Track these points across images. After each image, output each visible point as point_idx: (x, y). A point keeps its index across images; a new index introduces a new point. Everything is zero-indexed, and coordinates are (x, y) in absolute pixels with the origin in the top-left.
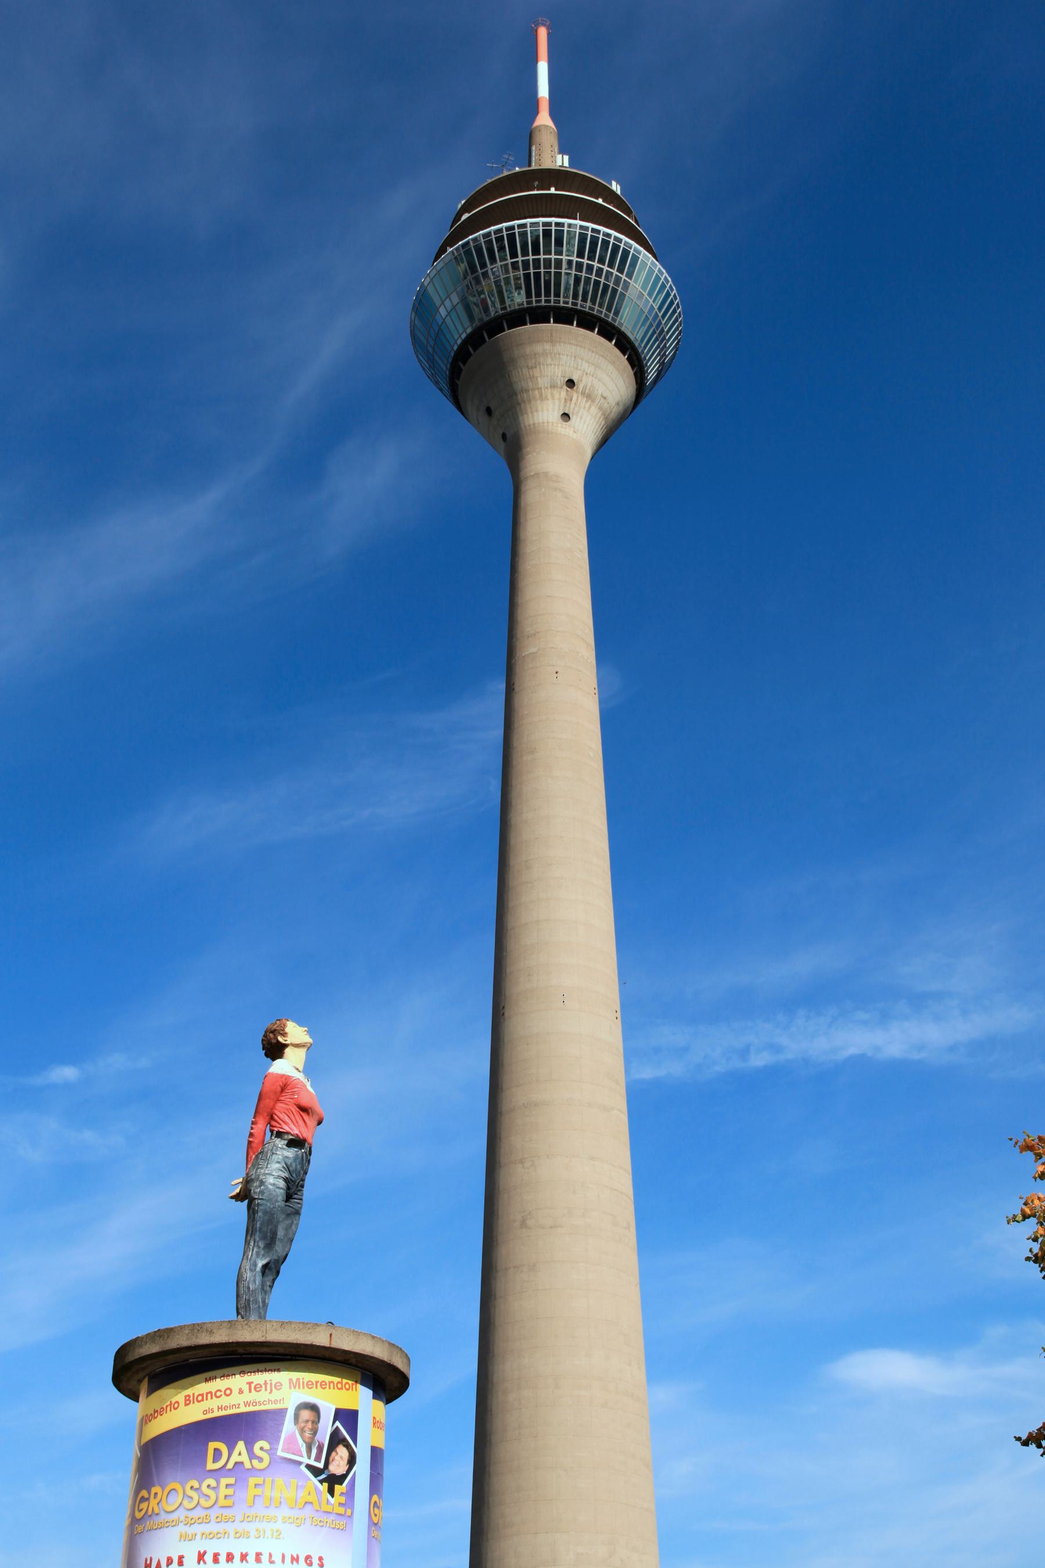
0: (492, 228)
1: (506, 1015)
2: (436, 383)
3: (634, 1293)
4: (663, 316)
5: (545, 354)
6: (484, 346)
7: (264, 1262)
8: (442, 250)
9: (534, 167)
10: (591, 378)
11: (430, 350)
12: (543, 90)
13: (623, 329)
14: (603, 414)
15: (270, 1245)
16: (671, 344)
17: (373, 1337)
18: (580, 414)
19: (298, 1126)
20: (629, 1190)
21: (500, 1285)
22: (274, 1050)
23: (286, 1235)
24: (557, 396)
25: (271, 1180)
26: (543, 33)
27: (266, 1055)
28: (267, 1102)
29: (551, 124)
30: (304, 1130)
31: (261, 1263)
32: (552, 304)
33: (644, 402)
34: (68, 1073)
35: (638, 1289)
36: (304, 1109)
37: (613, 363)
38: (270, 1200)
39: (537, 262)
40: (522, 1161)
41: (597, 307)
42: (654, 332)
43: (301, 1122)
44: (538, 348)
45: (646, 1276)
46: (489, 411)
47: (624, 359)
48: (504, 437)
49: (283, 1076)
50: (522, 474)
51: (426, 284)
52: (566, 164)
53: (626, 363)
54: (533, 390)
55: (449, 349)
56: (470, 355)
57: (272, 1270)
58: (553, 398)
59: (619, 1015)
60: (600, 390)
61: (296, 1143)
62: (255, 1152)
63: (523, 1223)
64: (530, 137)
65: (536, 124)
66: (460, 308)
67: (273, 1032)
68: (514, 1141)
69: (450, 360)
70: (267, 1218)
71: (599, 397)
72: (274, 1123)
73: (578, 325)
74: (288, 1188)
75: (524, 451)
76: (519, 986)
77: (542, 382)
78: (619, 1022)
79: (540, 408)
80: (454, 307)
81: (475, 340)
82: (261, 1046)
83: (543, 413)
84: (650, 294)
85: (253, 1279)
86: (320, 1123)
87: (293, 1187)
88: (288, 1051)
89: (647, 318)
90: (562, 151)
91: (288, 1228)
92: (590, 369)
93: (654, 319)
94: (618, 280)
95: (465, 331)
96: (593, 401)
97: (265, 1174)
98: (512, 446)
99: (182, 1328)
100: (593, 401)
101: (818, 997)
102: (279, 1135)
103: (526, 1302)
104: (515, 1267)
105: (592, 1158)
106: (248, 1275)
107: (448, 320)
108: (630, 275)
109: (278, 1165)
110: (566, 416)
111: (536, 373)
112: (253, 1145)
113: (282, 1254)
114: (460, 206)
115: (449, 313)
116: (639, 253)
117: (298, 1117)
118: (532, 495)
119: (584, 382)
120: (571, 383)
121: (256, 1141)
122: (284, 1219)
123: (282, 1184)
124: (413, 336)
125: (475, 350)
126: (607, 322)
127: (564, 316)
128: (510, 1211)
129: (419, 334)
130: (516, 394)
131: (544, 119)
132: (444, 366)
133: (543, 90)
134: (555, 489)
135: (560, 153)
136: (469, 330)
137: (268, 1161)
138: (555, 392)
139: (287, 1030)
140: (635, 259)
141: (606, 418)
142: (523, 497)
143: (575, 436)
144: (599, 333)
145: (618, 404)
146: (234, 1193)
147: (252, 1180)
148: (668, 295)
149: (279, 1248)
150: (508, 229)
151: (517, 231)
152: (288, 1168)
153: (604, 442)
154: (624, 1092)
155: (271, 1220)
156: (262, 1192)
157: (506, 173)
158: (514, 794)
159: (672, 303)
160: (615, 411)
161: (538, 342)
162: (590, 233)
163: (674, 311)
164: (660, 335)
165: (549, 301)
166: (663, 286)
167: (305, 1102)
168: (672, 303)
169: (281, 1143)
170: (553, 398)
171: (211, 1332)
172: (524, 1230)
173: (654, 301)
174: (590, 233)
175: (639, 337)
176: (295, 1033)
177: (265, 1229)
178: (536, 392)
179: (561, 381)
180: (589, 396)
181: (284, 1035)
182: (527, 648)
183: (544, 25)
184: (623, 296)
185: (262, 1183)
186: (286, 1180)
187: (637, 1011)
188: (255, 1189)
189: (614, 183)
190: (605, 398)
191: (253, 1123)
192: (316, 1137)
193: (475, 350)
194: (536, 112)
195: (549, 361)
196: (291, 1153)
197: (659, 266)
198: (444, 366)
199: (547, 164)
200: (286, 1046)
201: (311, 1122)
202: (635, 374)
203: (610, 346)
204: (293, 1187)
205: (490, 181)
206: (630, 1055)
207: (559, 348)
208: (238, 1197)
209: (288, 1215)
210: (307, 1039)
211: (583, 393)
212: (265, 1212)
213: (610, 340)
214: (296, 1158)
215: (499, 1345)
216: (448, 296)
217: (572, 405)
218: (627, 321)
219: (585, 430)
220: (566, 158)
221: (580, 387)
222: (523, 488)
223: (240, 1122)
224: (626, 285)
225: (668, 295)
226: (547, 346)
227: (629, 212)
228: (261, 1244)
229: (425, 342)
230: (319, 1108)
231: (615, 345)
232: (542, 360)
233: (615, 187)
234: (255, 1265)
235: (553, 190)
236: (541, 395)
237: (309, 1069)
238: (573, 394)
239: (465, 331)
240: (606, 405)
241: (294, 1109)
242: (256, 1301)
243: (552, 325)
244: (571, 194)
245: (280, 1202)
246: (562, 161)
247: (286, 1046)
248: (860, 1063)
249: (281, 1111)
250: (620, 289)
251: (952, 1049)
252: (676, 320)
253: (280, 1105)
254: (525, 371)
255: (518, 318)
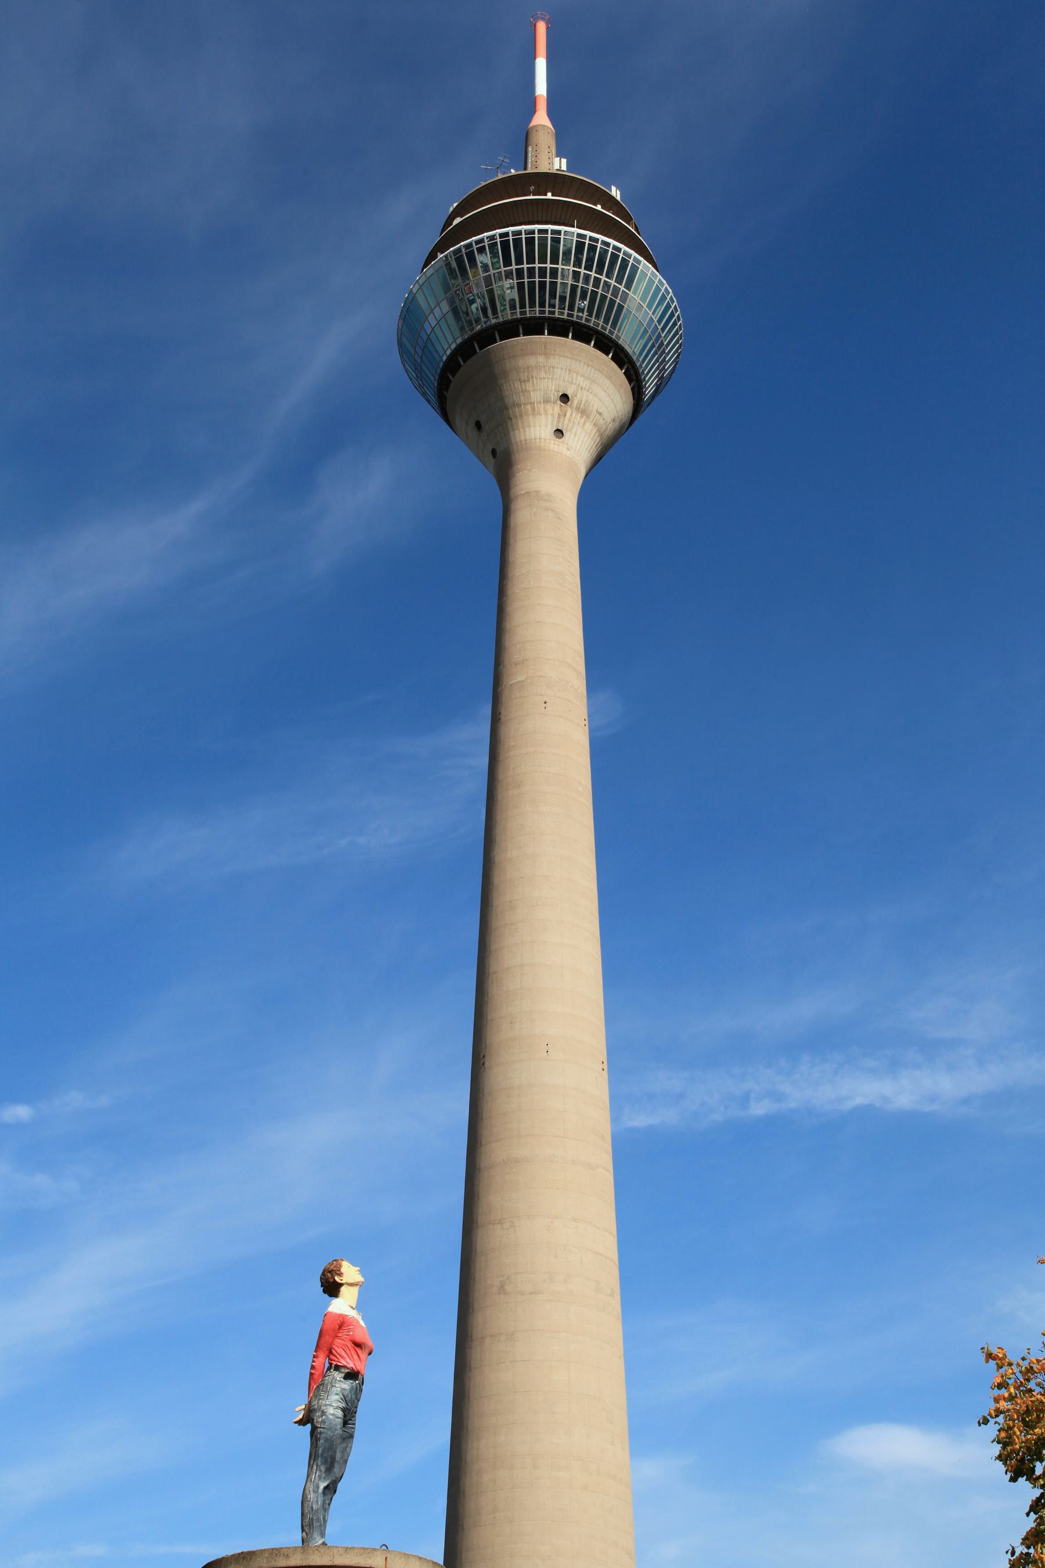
0: (486, 234)
1: (486, 1064)
2: (424, 394)
3: (617, 1365)
4: (663, 329)
5: (538, 367)
6: (474, 358)
7: (325, 1484)
8: (432, 256)
9: (529, 171)
10: (586, 393)
11: (419, 360)
12: (541, 88)
13: (620, 342)
14: (599, 430)
15: (329, 1469)
16: (671, 358)
17: (420, 1558)
18: (574, 431)
19: (351, 1357)
20: (613, 1253)
21: (475, 1355)
22: (332, 1288)
23: (342, 1457)
24: (550, 411)
25: (331, 1410)
26: (541, 27)
27: (324, 1292)
28: (327, 1338)
29: (548, 124)
30: (357, 1362)
31: (322, 1487)
32: (547, 315)
33: (640, 419)
34: (22, 1112)
35: (622, 1361)
36: (358, 1345)
37: (609, 378)
38: (330, 1429)
39: (531, 271)
40: (501, 1222)
41: (593, 319)
42: (653, 346)
43: (355, 1356)
44: (532, 361)
45: (630, 1339)
46: (478, 426)
47: (620, 373)
48: (494, 452)
49: (340, 1315)
50: (512, 492)
51: (414, 291)
52: (564, 168)
53: (624, 377)
54: (525, 404)
55: (438, 359)
56: (460, 366)
57: (331, 1489)
58: (546, 414)
59: (605, 1066)
60: (596, 405)
61: (352, 1375)
62: (316, 1384)
63: (502, 1289)
64: (526, 138)
65: (532, 124)
66: (450, 317)
67: (331, 1272)
68: (495, 1199)
69: (439, 371)
70: (327, 1445)
71: (594, 413)
72: (332, 1357)
73: (574, 338)
74: (345, 1416)
75: (515, 468)
76: (500, 1033)
77: (535, 396)
78: (605, 1074)
79: (532, 423)
80: (444, 316)
81: (465, 351)
82: (320, 1284)
83: (535, 429)
84: (649, 306)
85: (315, 1499)
86: (370, 1354)
87: (349, 1414)
88: (343, 1289)
89: (646, 331)
90: (559, 154)
91: (344, 1450)
92: (585, 384)
93: (653, 333)
94: (616, 290)
95: (455, 341)
96: (588, 417)
97: (326, 1405)
98: (502, 463)
99: (262, 1551)
100: (588, 417)
101: (824, 1042)
102: (337, 1368)
103: (501, 1375)
104: (492, 1336)
105: (575, 1220)
106: (311, 1496)
107: (437, 330)
108: (628, 286)
109: (337, 1397)
110: (559, 433)
111: (529, 386)
112: (315, 1376)
113: (338, 1475)
114: (451, 209)
115: (438, 322)
116: (639, 262)
117: (353, 1351)
118: (522, 514)
119: (579, 396)
120: (565, 398)
121: (317, 1373)
122: (341, 1443)
123: (340, 1413)
124: (400, 344)
125: (465, 362)
126: (604, 335)
127: (559, 329)
128: (488, 1274)
129: (406, 342)
130: (507, 408)
131: (541, 118)
132: (433, 378)
133: (541, 88)
134: (547, 509)
135: (557, 156)
136: (459, 341)
137: (328, 1392)
138: (549, 407)
139: (342, 1270)
140: (635, 269)
141: (601, 435)
142: (512, 517)
143: (568, 453)
144: (596, 346)
145: (614, 420)
146: (298, 1419)
147: (315, 1410)
148: (668, 306)
149: (336, 1469)
150: (502, 235)
151: (511, 238)
152: (345, 1399)
153: (599, 459)
154: (609, 1148)
155: (331, 1447)
156: (323, 1422)
157: (500, 176)
158: (498, 830)
159: (672, 315)
160: (611, 428)
161: (532, 354)
162: (587, 242)
163: (675, 324)
164: (660, 348)
165: (543, 312)
166: (664, 298)
167: (359, 1338)
168: (672, 315)
169: (338, 1376)
170: (546, 414)
171: (287, 1556)
172: (502, 1296)
173: (653, 314)
174: (587, 242)
175: (637, 350)
176: (350, 1273)
177: (326, 1455)
178: (529, 407)
179: (555, 395)
180: (584, 412)
181: (340, 1275)
182: (515, 676)
183: (543, 19)
184: (621, 307)
185: (323, 1413)
186: (344, 1410)
187: (624, 1056)
188: (318, 1418)
189: (614, 188)
190: (600, 414)
191: (314, 1356)
192: (368, 1367)
193: (465, 362)
194: (533, 111)
195: (543, 374)
196: (347, 1385)
197: (659, 277)
198: (433, 378)
199: (543, 168)
200: (341, 1285)
201: (363, 1355)
202: (633, 389)
203: (607, 360)
204: (349, 1414)
205: (484, 184)
206: (618, 1103)
207: (553, 361)
208: (301, 1422)
209: (344, 1439)
210: (359, 1278)
211: (578, 409)
212: (326, 1440)
213: (607, 354)
214: (352, 1389)
215: (474, 1422)
216: (438, 304)
217: (566, 421)
218: (627, 337)
219: (579, 447)
220: (564, 161)
221: (574, 402)
222: (513, 507)
223: (303, 1355)
224: (625, 296)
225: (668, 306)
226: (541, 359)
227: (628, 219)
228: (323, 1468)
229: (412, 351)
230: (370, 1341)
231: (612, 358)
232: (535, 374)
233: (615, 192)
234: (318, 1487)
235: (549, 196)
236: (533, 409)
237: (359, 1307)
238: (566, 408)
239: (455, 341)
240: (601, 421)
241: (350, 1345)
242: (318, 1520)
243: (545, 337)
244: (568, 197)
245: (339, 1431)
246: (560, 165)
247: (341, 1285)
248: (866, 1114)
249: (340, 1346)
250: (618, 301)
251: (966, 1101)
252: (676, 333)
253: (338, 1341)
254: (517, 385)
255: (510, 330)
